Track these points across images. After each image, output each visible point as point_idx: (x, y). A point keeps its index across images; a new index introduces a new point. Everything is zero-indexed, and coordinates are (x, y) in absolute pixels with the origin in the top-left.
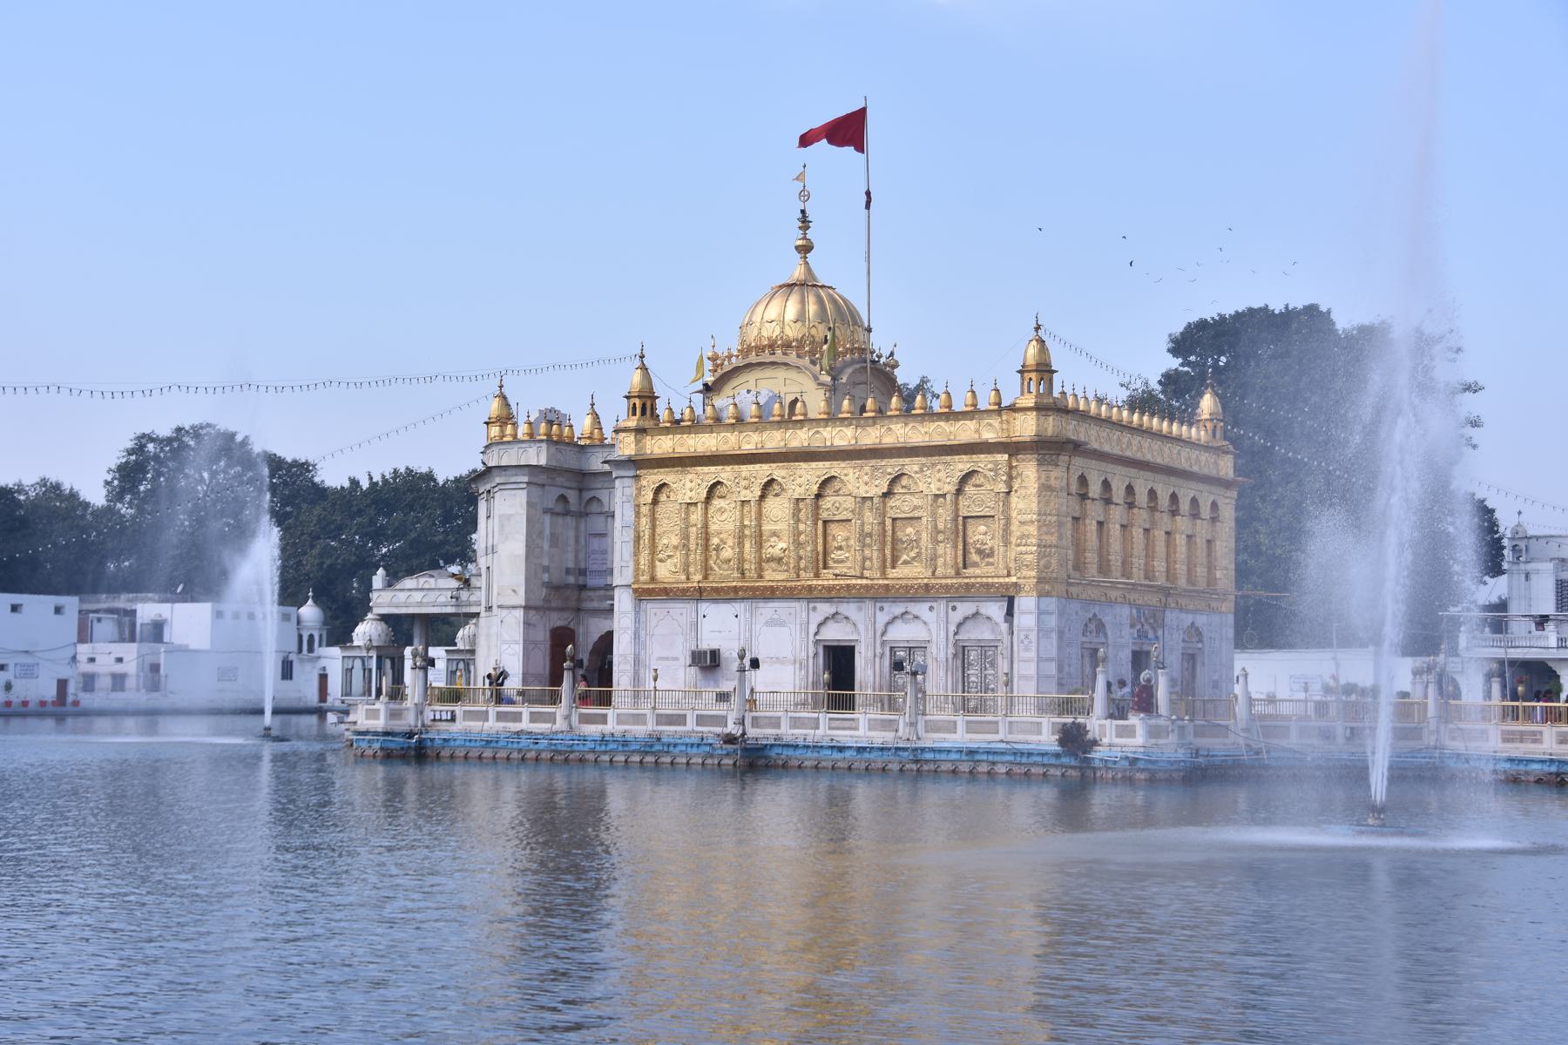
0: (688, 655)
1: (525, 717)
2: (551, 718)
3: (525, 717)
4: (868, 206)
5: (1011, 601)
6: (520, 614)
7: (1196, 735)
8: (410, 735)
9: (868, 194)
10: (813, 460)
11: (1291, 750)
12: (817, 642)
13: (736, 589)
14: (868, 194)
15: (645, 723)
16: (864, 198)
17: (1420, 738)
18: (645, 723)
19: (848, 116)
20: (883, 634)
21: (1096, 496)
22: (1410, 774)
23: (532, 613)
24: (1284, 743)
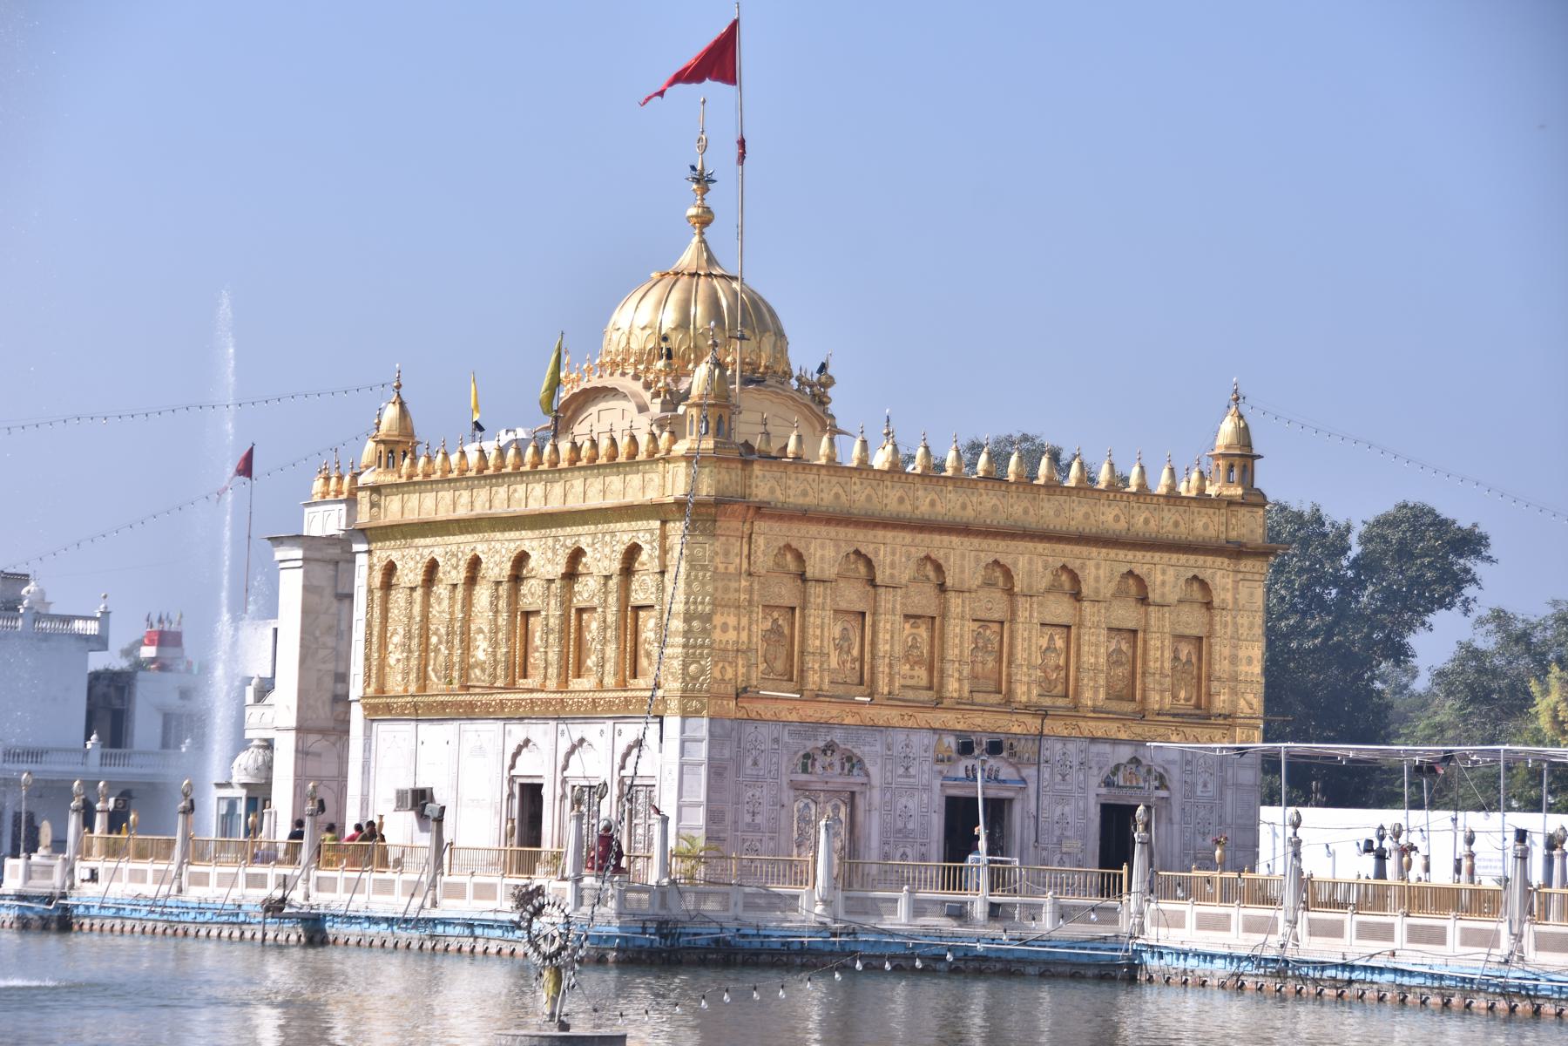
0: (393, 796)
1: (1191, 920)
2: (1491, 940)
3: (1191, 920)
4: (742, 156)
5: (661, 718)
6: (293, 734)
7: (747, 906)
8: (49, 899)
9: (742, 143)
10: (562, 525)
11: (891, 933)
12: (512, 779)
13: (443, 705)
14: (742, 143)
15: (264, 886)
16: (735, 150)
17: (1116, 922)
18: (264, 886)
19: (717, 42)
20: (512, 767)
21: (831, 572)
22: (1090, 973)
23: (312, 738)
24: (887, 923)
